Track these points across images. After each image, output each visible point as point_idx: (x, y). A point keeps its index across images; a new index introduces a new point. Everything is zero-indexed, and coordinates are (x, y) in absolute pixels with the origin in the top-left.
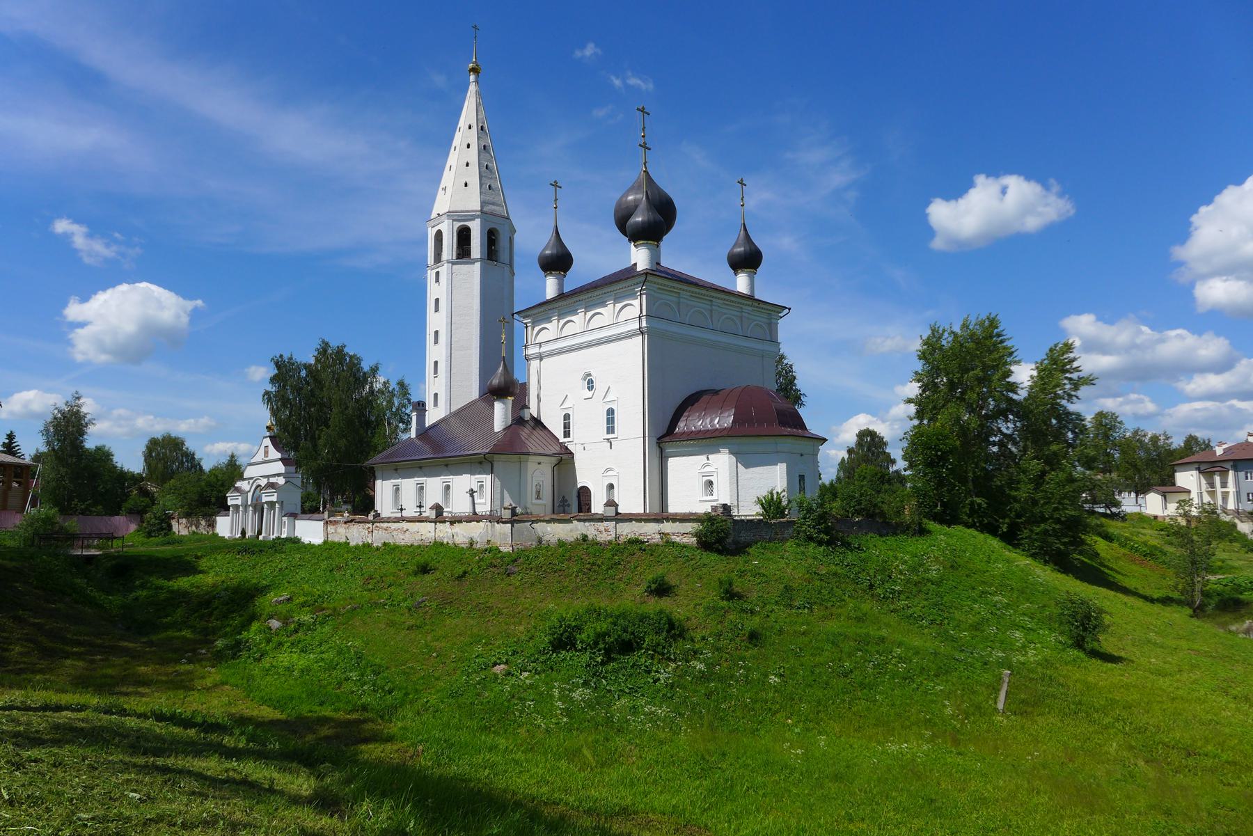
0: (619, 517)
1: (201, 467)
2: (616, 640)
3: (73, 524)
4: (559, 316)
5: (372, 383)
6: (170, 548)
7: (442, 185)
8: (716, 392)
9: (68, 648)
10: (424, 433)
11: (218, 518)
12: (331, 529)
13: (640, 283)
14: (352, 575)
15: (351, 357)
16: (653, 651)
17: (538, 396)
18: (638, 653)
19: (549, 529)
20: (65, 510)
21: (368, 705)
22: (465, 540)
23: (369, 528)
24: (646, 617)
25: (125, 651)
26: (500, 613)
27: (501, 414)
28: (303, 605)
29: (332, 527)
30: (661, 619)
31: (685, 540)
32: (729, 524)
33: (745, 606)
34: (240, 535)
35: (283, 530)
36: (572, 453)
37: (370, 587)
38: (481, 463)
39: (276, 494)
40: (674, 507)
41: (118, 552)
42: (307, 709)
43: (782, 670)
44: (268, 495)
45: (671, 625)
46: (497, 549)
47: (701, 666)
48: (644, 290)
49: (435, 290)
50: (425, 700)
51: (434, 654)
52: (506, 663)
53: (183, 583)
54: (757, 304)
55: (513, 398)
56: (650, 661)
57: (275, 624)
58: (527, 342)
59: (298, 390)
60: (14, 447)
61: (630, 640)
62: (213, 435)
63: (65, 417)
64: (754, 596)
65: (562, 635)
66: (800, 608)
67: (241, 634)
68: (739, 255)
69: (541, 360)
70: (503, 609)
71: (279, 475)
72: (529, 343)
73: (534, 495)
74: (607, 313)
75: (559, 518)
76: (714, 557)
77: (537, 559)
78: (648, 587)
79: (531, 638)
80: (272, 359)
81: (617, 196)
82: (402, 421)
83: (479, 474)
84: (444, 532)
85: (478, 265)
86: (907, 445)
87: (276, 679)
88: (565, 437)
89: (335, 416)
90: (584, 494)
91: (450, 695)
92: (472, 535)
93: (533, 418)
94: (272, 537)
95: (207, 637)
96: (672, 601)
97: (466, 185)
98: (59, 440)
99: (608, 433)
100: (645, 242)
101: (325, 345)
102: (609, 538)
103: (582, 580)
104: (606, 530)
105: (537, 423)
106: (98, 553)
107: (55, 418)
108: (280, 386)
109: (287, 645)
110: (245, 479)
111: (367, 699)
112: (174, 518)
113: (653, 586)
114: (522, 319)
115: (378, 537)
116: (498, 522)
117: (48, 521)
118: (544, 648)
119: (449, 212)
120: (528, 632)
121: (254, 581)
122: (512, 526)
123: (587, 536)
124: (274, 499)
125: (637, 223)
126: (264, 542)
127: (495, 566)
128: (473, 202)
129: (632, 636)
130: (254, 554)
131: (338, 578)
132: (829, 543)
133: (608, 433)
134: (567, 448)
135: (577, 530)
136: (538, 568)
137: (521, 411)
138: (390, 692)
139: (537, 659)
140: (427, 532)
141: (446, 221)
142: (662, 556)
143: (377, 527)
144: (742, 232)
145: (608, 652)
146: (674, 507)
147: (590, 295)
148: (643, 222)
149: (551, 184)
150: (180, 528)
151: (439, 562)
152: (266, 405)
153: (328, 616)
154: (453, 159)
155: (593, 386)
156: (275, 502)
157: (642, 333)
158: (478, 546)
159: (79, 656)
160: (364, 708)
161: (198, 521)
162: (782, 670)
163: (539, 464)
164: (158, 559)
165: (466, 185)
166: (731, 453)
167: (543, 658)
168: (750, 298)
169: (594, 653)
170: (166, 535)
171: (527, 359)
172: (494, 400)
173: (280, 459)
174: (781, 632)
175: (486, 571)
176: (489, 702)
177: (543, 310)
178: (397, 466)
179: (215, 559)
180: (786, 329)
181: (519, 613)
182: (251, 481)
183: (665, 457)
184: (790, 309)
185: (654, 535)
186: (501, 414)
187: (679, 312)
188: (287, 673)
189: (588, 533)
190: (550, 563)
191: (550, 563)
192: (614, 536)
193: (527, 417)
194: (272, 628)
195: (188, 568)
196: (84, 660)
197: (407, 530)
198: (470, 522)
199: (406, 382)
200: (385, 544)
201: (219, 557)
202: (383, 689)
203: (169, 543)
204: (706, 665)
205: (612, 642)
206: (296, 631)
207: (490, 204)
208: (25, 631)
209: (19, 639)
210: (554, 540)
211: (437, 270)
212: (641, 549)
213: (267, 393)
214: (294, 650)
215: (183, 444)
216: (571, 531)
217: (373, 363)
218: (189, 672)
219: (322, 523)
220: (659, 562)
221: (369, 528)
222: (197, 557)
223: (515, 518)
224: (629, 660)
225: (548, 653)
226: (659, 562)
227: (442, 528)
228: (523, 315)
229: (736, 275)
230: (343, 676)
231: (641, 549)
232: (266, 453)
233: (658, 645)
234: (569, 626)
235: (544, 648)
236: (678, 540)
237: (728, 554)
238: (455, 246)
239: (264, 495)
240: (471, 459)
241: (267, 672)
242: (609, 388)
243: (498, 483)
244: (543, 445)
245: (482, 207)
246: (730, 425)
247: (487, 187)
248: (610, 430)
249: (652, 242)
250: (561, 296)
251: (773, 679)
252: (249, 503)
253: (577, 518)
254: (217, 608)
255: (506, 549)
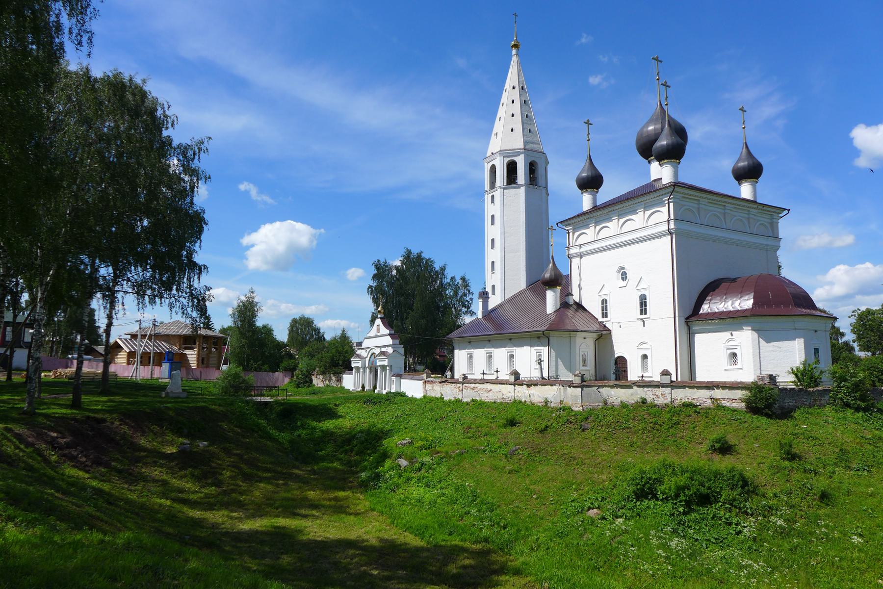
0: (674, 384)
1: (324, 339)
2: (695, 493)
3: (251, 377)
4: (618, 216)
5: (441, 279)
6: (315, 397)
7: (494, 132)
8: (734, 280)
9: (260, 473)
10: (488, 315)
11: (344, 376)
12: (429, 386)
13: (668, 193)
14: (453, 425)
15: (427, 260)
16: (731, 504)
17: (580, 286)
18: (715, 506)
19: (613, 393)
20: (247, 369)
21: (489, 538)
22: (540, 399)
23: (460, 387)
24: (720, 474)
25: (297, 478)
26: (583, 463)
27: (552, 299)
28: (422, 448)
29: (430, 385)
30: (734, 476)
31: (734, 405)
32: (776, 391)
33: (808, 467)
34: (360, 389)
35: (392, 386)
36: (609, 330)
37: (470, 435)
38: (539, 338)
39: (387, 360)
40: (701, 376)
41: (284, 400)
42: (442, 538)
43: (860, 530)
44: (383, 360)
45: (745, 482)
46: (570, 408)
47: (780, 522)
48: (672, 198)
49: (490, 210)
50: (535, 537)
51: (535, 496)
52: (599, 508)
53: (329, 424)
54: (761, 207)
55: (560, 288)
56: (729, 514)
57: (403, 462)
58: (569, 244)
59: (391, 284)
60: (210, 325)
61: (708, 494)
62: (325, 316)
63: (244, 305)
64: (811, 457)
65: (644, 486)
66: (858, 470)
67: (377, 468)
68: (743, 168)
69: (581, 257)
70: (585, 459)
71: (388, 346)
72: (571, 245)
73: (581, 363)
74: (638, 219)
75: (621, 384)
76: (764, 420)
77: (605, 417)
78: (712, 446)
79: (614, 487)
80: (373, 263)
81: (638, 129)
82: (464, 306)
83: (538, 346)
84: (522, 393)
85: (523, 189)
86: (855, 321)
87: (411, 509)
88: (603, 317)
89: (417, 304)
90: (621, 364)
91: (557, 535)
92: (546, 396)
93: (576, 303)
94: (384, 392)
95: (352, 468)
96: (735, 459)
97: (512, 130)
98: (241, 321)
99: (641, 313)
100: (670, 161)
101: (409, 252)
102: (666, 401)
103: (648, 437)
104: (662, 395)
105: (579, 306)
106: (271, 400)
107: (239, 306)
108: (378, 282)
109: (414, 480)
110: (363, 349)
111: (486, 533)
112: (314, 375)
113: (717, 446)
114: (564, 227)
115: (449, 392)
116: (569, 387)
117: (236, 376)
118: (628, 496)
119: (500, 151)
120: (611, 480)
121: (379, 426)
122: (582, 390)
123: (646, 400)
124: (386, 363)
125: (662, 146)
126: (380, 396)
127: (571, 422)
128: (518, 143)
129: (709, 491)
130: (375, 404)
131: (443, 427)
132: (865, 410)
133: (641, 313)
134: (605, 326)
135: (637, 394)
136: (608, 426)
137: (567, 297)
138: (505, 527)
139: (625, 506)
140: (508, 393)
141: (499, 158)
142: (716, 419)
143: (466, 387)
144: (744, 149)
145: (688, 504)
146: (701, 376)
147: (622, 206)
148: (668, 145)
149: (585, 123)
150: (318, 381)
151: (522, 417)
152: (370, 295)
153: (442, 458)
154: (502, 112)
155: (626, 278)
156: (387, 366)
157: (671, 234)
158: (553, 405)
159: (267, 480)
160: (486, 540)
161: (330, 377)
162: (860, 530)
163: (585, 338)
164: (310, 406)
165: (512, 130)
166: (753, 330)
167: (630, 505)
168: (754, 202)
169: (676, 504)
170: (309, 386)
171: (570, 257)
172: (546, 289)
173: (389, 334)
174: (849, 493)
175: (563, 426)
176: (593, 544)
177: (581, 220)
178: (470, 339)
179: (349, 407)
180: (785, 227)
181: (600, 464)
182: (368, 350)
183: (692, 333)
184: (789, 210)
185: (705, 400)
186: (552, 299)
187: (699, 215)
188: (418, 504)
189: (647, 397)
190: (618, 422)
191: (618, 422)
192: (670, 400)
193: (571, 302)
194: (401, 465)
195: (331, 414)
196: (272, 484)
197: (491, 390)
198: (545, 385)
199: (467, 278)
200: (473, 400)
201: (351, 406)
202: (498, 524)
203: (314, 393)
204: (785, 520)
205: (691, 495)
206: (420, 470)
207: (531, 143)
208: (232, 460)
209: (229, 466)
210: (617, 402)
211: (492, 194)
212: (696, 412)
213: (370, 287)
214: (420, 484)
215: (313, 323)
216: (632, 395)
217: (442, 264)
218: (347, 498)
219: (422, 382)
220: (715, 423)
221: (460, 387)
222: (336, 405)
223: (584, 383)
224: (710, 510)
225: (632, 501)
226: (715, 423)
227: (520, 389)
228: (566, 223)
229: (740, 185)
230: (464, 510)
231: (696, 412)
232: (378, 330)
233: (734, 500)
234: (650, 479)
235: (628, 496)
236: (728, 404)
237: (777, 418)
238: (505, 176)
239: (378, 360)
240: (530, 335)
241: (403, 501)
242: (641, 278)
243: (553, 353)
244: (583, 324)
245: (525, 145)
246: (751, 307)
247: (528, 131)
248: (643, 311)
249: (675, 161)
250: (595, 208)
251: (856, 540)
252: (367, 366)
253: (637, 384)
254: (356, 446)
255: (577, 408)
